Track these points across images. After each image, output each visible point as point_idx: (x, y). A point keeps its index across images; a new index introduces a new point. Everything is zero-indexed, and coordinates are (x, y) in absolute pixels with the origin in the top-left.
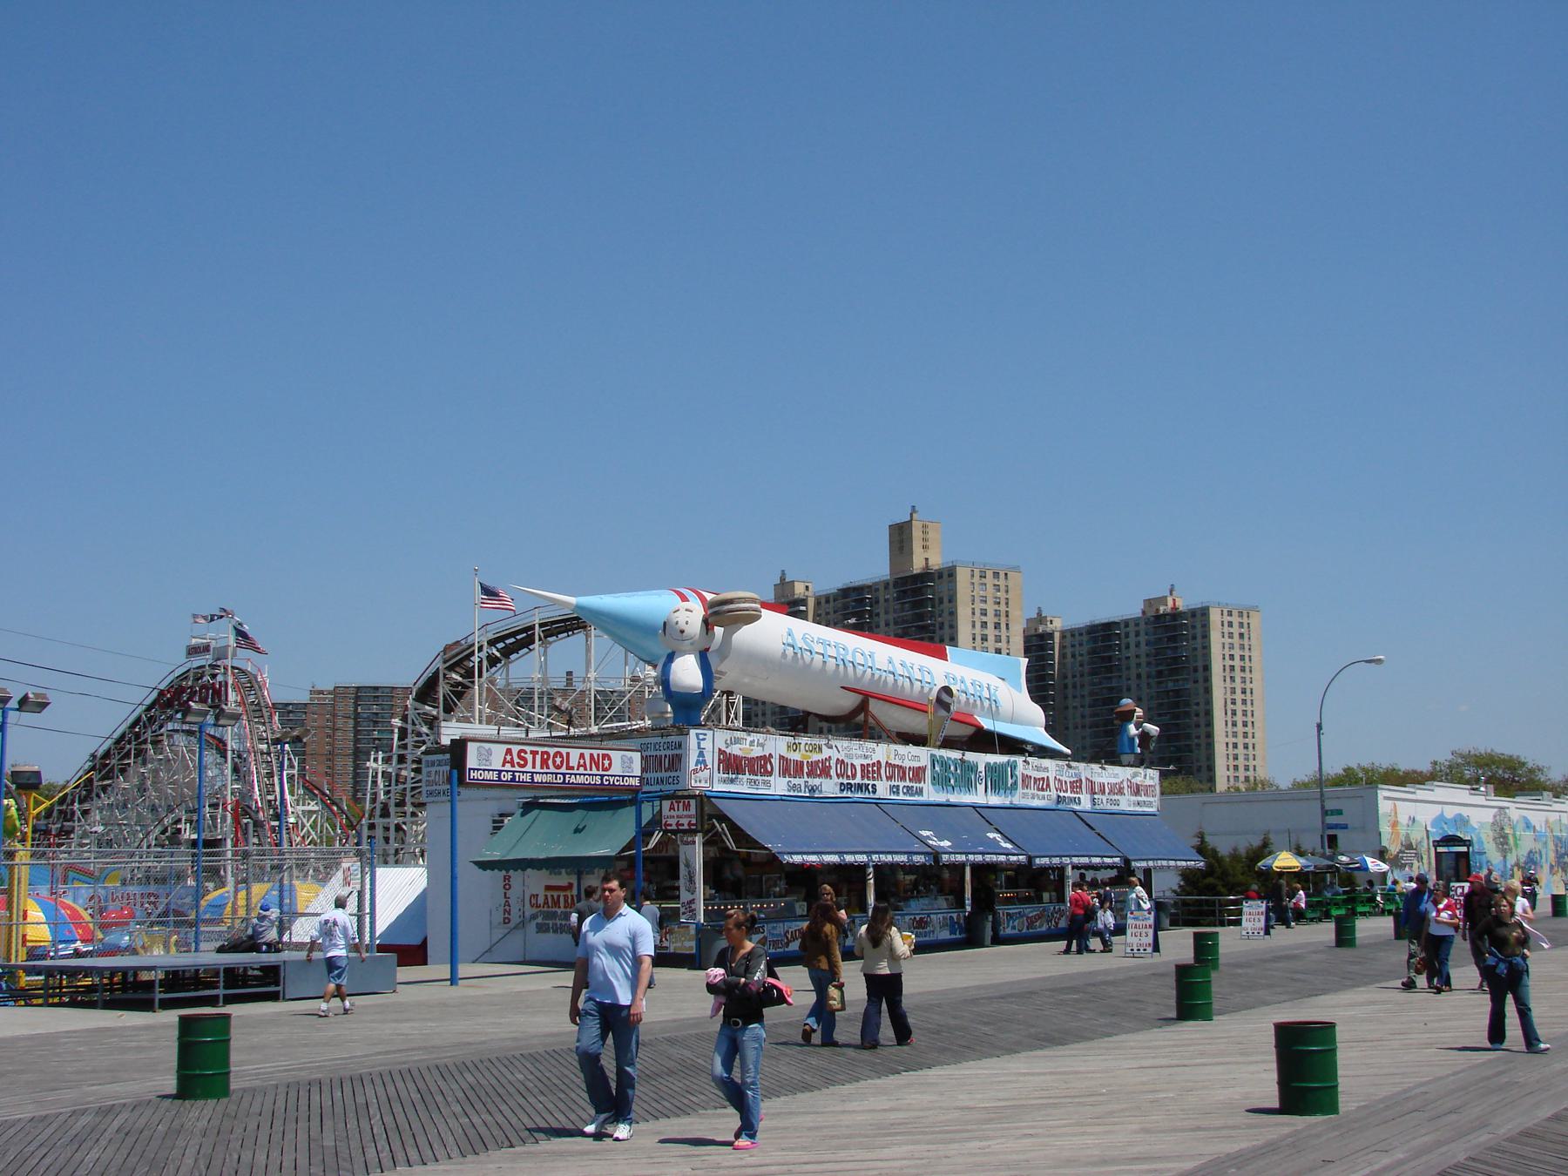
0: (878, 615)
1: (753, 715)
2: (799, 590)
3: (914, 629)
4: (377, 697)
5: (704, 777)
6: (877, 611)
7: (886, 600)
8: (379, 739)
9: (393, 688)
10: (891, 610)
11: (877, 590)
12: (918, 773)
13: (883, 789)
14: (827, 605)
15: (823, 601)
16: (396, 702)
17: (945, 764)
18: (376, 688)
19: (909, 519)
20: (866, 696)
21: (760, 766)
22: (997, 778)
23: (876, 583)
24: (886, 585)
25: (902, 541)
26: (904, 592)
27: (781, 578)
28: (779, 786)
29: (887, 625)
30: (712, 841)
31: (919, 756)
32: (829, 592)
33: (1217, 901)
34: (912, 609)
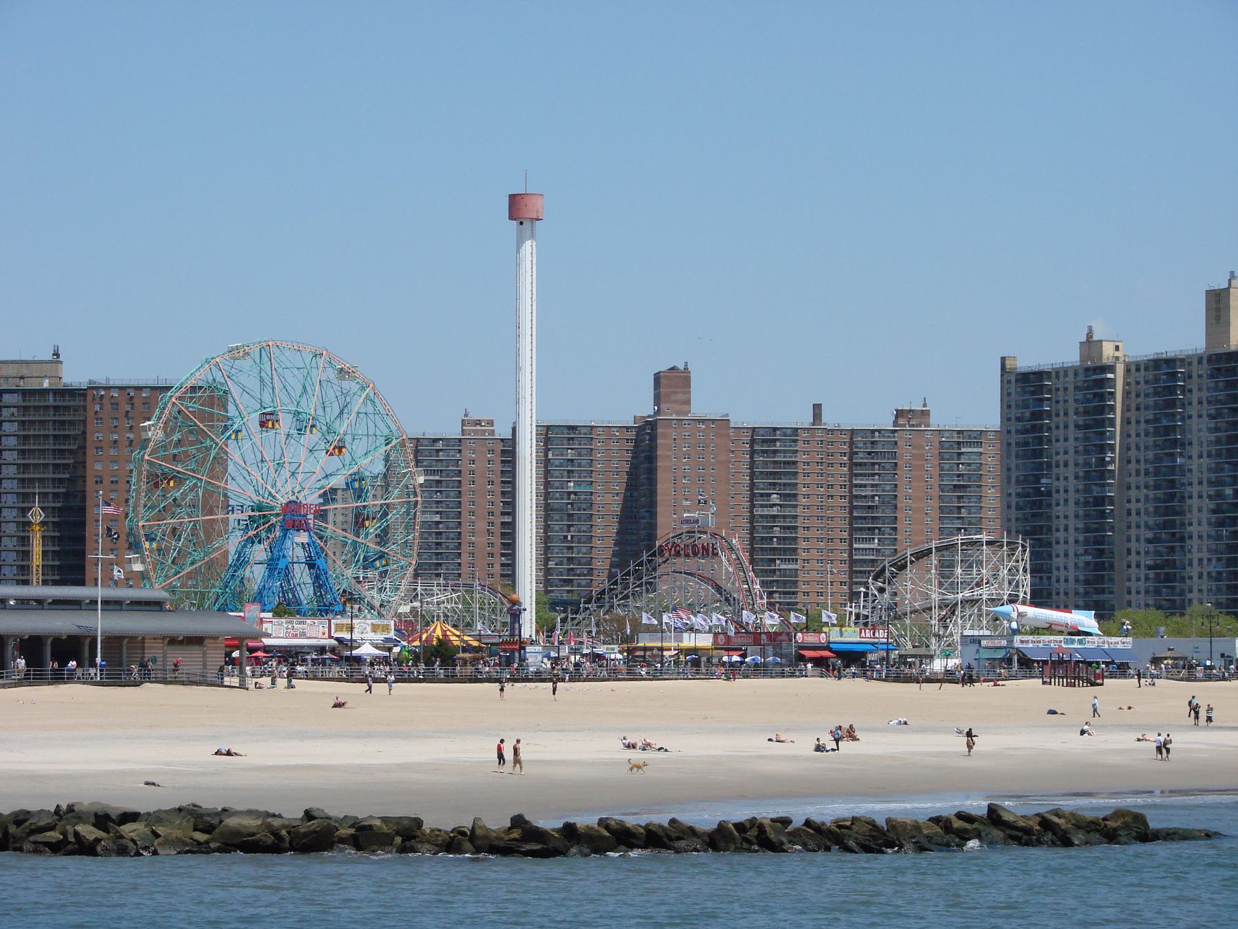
0: (1190, 391)
1: (1054, 491)
2: (1108, 351)
3: (1226, 411)
4: (572, 439)
5: (1017, 644)
6: (1189, 387)
7: (1200, 376)
8: (575, 493)
9: (592, 427)
10: (1205, 388)
11: (1190, 364)
12: (1061, 642)
13: (1052, 645)
14: (1137, 374)
15: (1133, 368)
16: (596, 446)
17: (1067, 639)
18: (572, 428)
19: (1227, 286)
20: (1051, 624)
21: (1027, 642)
22: (1080, 642)
23: (1188, 356)
24: (1200, 360)
25: (1218, 310)
26: (1218, 369)
27: (1087, 334)
28: (1031, 645)
29: (1200, 403)
30: (1018, 655)
31: (1062, 638)
32: (1139, 359)
33: (36, 575)
34: (1226, 388)
